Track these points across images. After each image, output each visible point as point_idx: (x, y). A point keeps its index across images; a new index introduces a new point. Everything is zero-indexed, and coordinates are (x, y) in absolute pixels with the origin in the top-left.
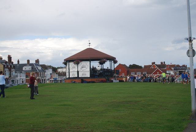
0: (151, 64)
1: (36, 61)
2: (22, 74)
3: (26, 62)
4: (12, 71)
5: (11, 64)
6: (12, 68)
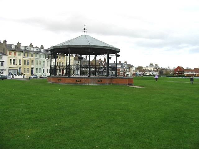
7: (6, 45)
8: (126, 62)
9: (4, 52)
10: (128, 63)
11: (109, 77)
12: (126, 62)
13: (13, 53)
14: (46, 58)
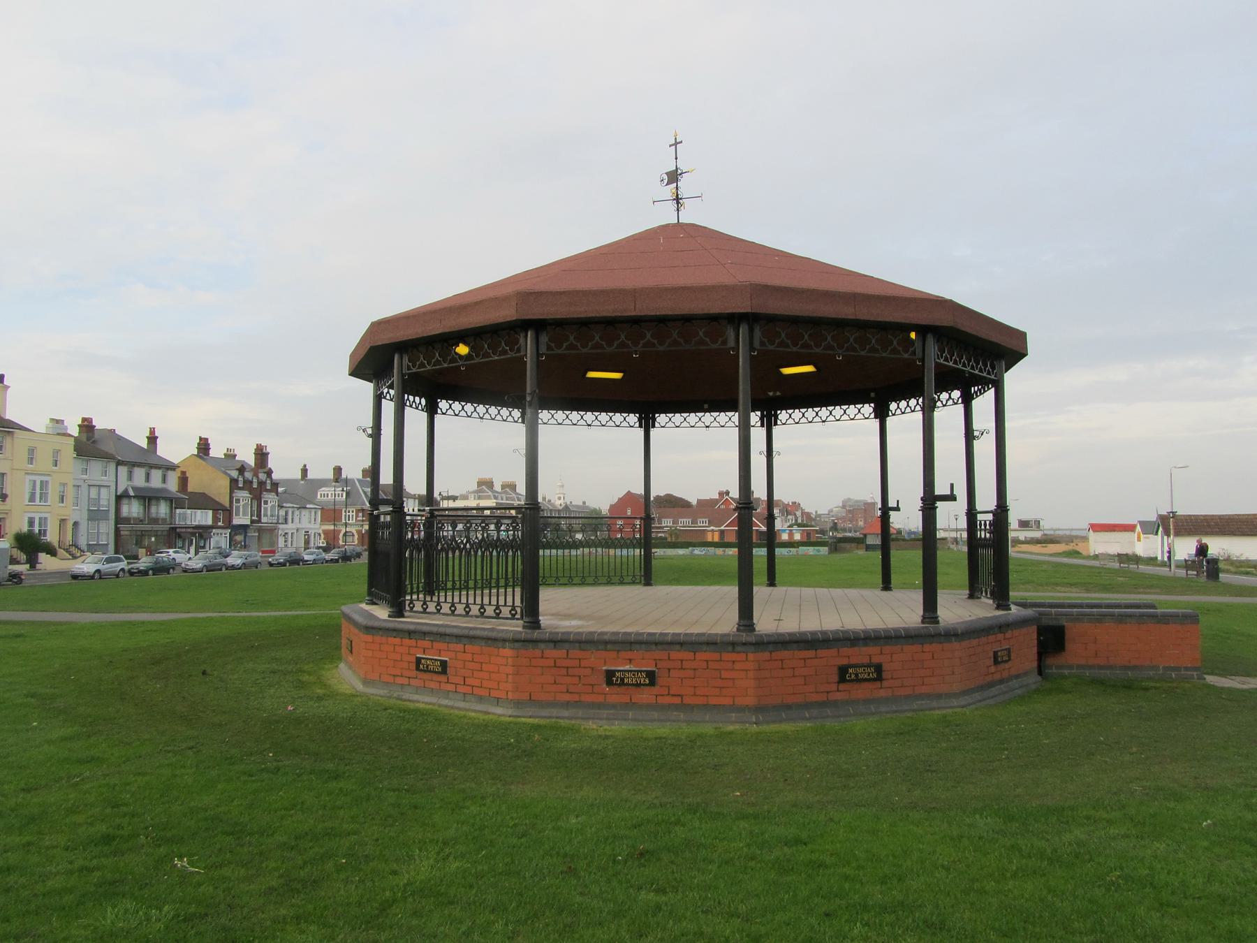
0: (717, 497)
1: (480, 483)
2: (304, 512)
3: (330, 475)
4: (266, 503)
5: (262, 476)
6: (267, 491)
11: (410, 620)
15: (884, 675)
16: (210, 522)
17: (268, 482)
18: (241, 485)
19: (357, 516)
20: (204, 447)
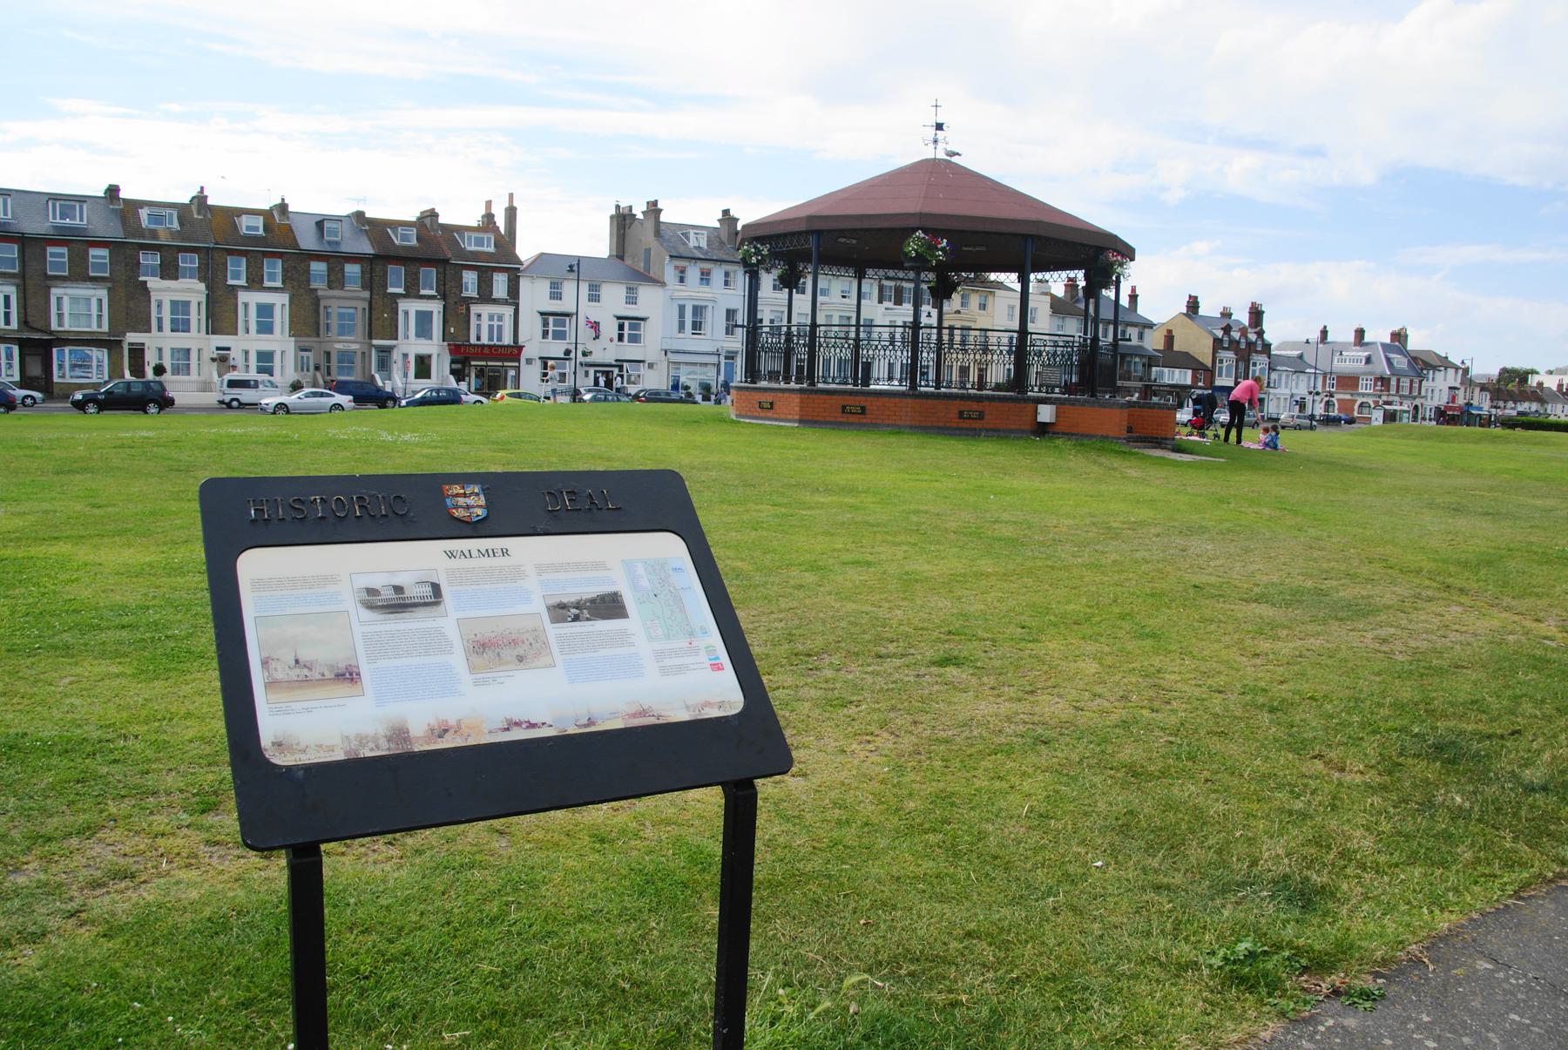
4: (1255, 364)
6: (1257, 352)
7: (659, 229)
8: (1399, 337)
9: (647, 267)
10: (1412, 345)
11: (758, 385)
12: (1399, 337)
13: (693, 272)
14: (880, 302)
15: (867, 412)
16: (1189, 382)
17: (1259, 342)
18: (1226, 345)
19: (1375, 385)
20: (1193, 305)
